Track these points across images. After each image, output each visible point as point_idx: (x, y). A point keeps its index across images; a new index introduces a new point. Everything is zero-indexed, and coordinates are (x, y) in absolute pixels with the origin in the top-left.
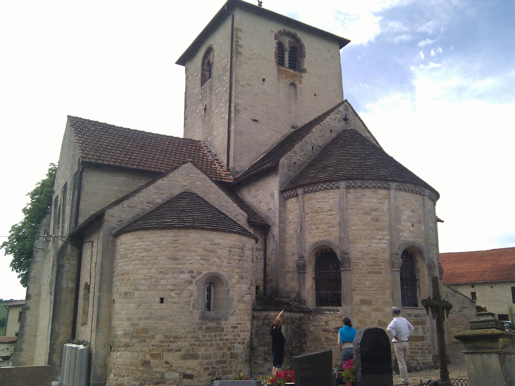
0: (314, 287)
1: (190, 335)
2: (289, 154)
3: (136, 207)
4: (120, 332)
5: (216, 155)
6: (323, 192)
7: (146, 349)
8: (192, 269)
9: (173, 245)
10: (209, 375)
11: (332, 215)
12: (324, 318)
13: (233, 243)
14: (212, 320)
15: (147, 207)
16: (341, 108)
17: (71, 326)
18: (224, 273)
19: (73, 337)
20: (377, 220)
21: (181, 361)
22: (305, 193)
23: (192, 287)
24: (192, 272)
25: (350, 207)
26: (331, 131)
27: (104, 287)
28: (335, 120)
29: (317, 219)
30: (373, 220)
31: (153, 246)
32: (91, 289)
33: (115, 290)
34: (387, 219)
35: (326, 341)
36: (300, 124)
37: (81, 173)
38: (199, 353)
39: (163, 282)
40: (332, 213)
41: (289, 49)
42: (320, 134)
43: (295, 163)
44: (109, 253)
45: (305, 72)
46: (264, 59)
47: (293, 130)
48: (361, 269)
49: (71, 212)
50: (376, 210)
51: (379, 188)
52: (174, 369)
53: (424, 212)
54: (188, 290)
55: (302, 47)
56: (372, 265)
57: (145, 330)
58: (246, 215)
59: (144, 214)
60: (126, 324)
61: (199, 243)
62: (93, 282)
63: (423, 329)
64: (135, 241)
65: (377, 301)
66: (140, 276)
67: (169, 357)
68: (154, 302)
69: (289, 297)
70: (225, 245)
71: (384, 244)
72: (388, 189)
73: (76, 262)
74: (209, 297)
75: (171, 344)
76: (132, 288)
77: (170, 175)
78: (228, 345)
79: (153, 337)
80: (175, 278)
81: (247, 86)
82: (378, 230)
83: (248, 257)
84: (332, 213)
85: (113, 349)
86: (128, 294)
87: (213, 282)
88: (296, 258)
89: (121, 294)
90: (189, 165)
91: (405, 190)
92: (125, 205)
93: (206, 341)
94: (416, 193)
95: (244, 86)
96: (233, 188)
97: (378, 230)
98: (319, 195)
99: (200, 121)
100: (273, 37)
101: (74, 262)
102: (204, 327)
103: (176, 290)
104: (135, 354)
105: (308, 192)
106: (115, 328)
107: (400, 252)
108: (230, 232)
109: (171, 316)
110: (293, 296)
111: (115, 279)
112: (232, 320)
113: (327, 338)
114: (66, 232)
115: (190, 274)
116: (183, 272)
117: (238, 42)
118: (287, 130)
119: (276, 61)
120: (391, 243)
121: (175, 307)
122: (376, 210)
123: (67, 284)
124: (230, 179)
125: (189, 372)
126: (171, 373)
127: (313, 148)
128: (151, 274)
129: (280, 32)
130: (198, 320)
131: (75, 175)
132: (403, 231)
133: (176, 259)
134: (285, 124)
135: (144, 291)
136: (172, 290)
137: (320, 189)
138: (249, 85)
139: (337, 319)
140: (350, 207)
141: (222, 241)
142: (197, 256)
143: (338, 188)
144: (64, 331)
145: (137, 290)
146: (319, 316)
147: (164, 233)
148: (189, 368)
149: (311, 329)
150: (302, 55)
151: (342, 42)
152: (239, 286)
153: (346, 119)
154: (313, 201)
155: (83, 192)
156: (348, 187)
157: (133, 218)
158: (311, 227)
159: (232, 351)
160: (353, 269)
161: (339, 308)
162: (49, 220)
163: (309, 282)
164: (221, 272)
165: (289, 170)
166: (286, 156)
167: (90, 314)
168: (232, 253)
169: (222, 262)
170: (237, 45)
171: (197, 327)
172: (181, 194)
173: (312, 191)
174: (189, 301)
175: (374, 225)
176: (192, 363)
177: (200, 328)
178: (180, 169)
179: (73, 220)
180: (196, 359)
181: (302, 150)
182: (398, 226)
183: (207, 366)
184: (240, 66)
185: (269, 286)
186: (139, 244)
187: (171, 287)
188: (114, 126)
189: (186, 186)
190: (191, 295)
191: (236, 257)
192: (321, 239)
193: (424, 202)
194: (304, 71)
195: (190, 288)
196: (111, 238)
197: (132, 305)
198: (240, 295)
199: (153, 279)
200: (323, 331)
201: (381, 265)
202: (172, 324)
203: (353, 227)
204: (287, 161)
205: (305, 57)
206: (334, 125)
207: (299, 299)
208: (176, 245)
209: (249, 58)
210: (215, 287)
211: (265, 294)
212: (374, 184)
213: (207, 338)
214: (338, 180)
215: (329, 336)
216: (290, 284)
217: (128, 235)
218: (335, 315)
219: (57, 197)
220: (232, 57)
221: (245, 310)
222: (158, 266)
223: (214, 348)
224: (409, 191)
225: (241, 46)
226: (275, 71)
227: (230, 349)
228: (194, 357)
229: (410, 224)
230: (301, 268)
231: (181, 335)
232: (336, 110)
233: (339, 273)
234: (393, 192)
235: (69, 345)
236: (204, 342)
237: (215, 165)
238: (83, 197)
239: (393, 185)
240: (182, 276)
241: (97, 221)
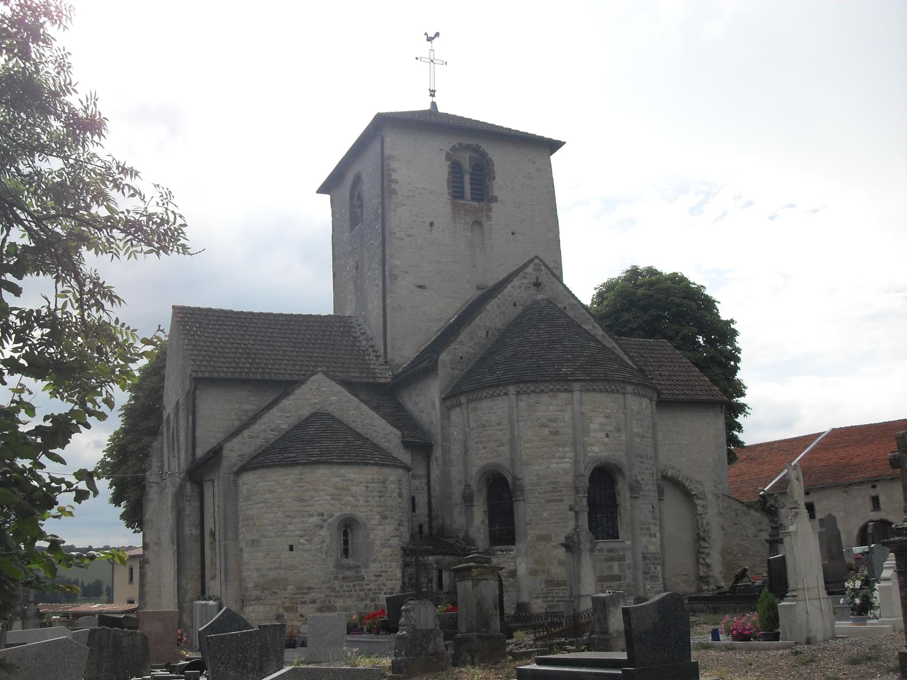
0: (487, 522)
1: (325, 586)
2: (453, 346)
3: (258, 437)
4: (250, 585)
5: (371, 339)
11: (501, 430)
13: (370, 476)
14: (350, 568)
16: (530, 269)
17: (200, 580)
18: (361, 514)
19: (203, 594)
20: (557, 433)
22: (469, 401)
23: (323, 532)
24: (322, 514)
26: (515, 305)
30: (551, 433)
32: (217, 537)
33: (241, 537)
34: (570, 431)
36: (491, 282)
37: (194, 393)
38: (337, 605)
39: (290, 527)
40: (501, 427)
41: (470, 170)
43: (461, 358)
44: (232, 494)
45: (496, 201)
47: (480, 293)
48: (537, 498)
49: (187, 442)
50: (555, 420)
51: (558, 390)
53: (625, 415)
56: (550, 492)
58: (399, 433)
59: (268, 445)
61: (328, 480)
62: (217, 528)
63: (620, 566)
65: (558, 535)
67: (302, 609)
69: (457, 536)
71: (567, 464)
72: (571, 391)
73: (198, 504)
74: (346, 542)
75: (305, 596)
78: (371, 595)
79: (285, 589)
80: (303, 522)
83: (393, 492)
84: (501, 427)
87: (348, 527)
90: (320, 376)
91: (594, 390)
94: (613, 391)
95: (402, 239)
96: (387, 395)
97: (558, 446)
98: (485, 404)
100: (444, 158)
101: (196, 504)
102: (340, 576)
105: (472, 400)
107: (588, 474)
108: (366, 464)
110: (462, 535)
111: (240, 525)
112: (375, 567)
114: (184, 466)
116: (312, 515)
117: (390, 175)
118: (470, 294)
120: (576, 462)
122: (555, 420)
123: (190, 530)
124: (386, 377)
127: (487, 332)
129: (454, 149)
131: (187, 394)
132: (592, 445)
134: (468, 285)
136: (301, 536)
137: (486, 397)
141: (356, 476)
142: (327, 495)
143: (506, 394)
144: (192, 586)
145: (264, 537)
147: (289, 470)
152: (382, 527)
153: (537, 284)
155: (198, 416)
156: (518, 393)
157: (255, 451)
159: (377, 602)
162: (162, 442)
163: (479, 515)
164: (357, 513)
165: (453, 369)
166: (448, 349)
167: (218, 566)
168: (370, 489)
169: (358, 501)
170: (391, 181)
172: (314, 414)
173: (476, 399)
177: (336, 578)
178: (309, 382)
179: (190, 453)
182: (586, 439)
185: (434, 524)
188: (232, 312)
190: (323, 542)
191: (375, 493)
192: (489, 461)
193: (625, 403)
194: (495, 199)
196: (232, 476)
198: (384, 539)
202: (305, 573)
203: (526, 445)
205: (494, 178)
209: (408, 197)
210: (352, 531)
211: (431, 534)
212: (551, 387)
213: (345, 588)
216: (457, 520)
217: (250, 473)
219: (169, 416)
220: (383, 199)
221: (391, 555)
224: (601, 391)
225: (396, 181)
226: (448, 208)
227: (373, 600)
228: (332, 609)
229: (603, 435)
230: (468, 499)
232: (522, 274)
233: (512, 503)
234: (577, 395)
235: (199, 602)
236: (342, 593)
237: (369, 355)
238: (199, 421)
239: (577, 386)
240: (311, 520)
241: (216, 454)
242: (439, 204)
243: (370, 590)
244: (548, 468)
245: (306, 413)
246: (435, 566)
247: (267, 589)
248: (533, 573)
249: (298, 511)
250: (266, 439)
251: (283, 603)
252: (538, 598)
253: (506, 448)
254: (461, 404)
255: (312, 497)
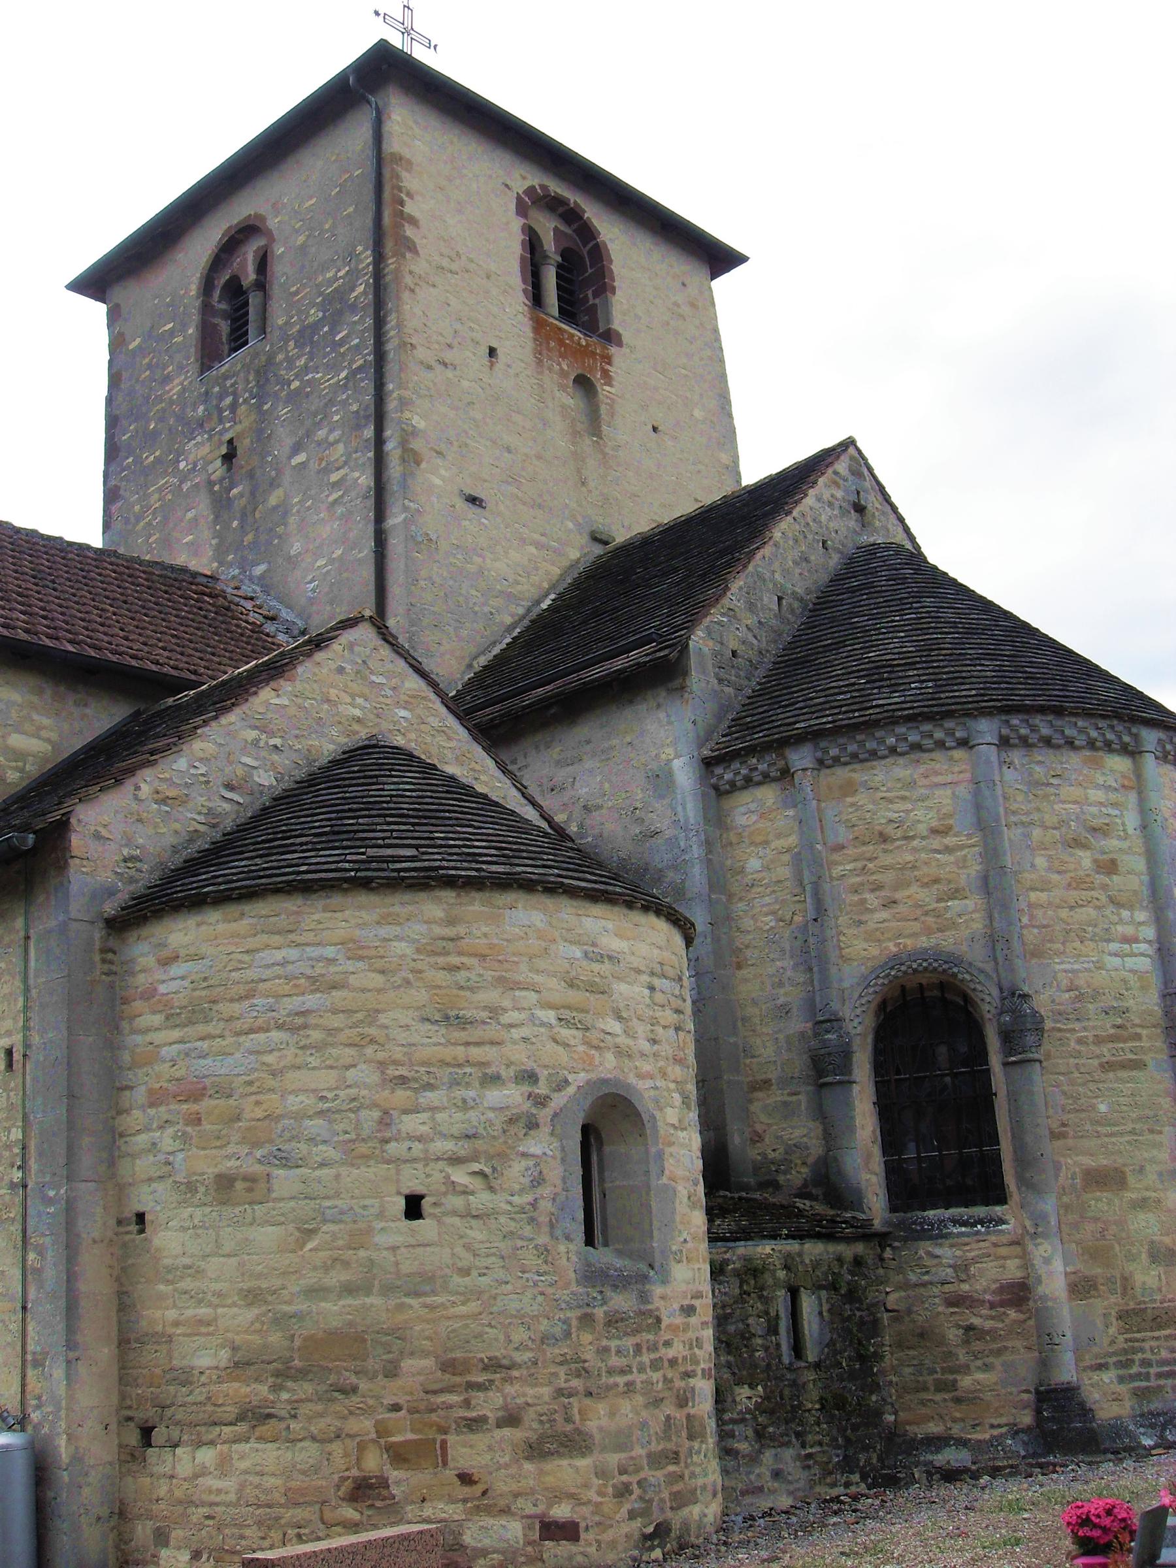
2: (716, 615)
6: (901, 761)
7: (366, 1425)
8: (530, 1065)
9: (441, 960)
10: (632, 1515)
11: (948, 850)
12: (946, 1253)
14: (621, 1282)
15: (227, 806)
16: (842, 466)
21: (528, 1466)
23: (539, 1145)
24: (531, 1077)
25: (1013, 819)
27: (87, 1161)
28: (830, 504)
29: (886, 868)
31: (350, 966)
34: (1140, 865)
35: (967, 1342)
38: (592, 1426)
39: (411, 1124)
40: (950, 841)
42: (796, 554)
43: (734, 654)
45: (620, 344)
46: (488, 277)
47: (598, 550)
48: (1078, 1055)
51: (1108, 746)
52: (502, 1503)
54: (524, 1155)
55: (598, 254)
56: (1112, 1039)
57: (350, 1342)
60: (239, 1319)
64: (252, 943)
66: (294, 1102)
67: (468, 1452)
68: (381, 1215)
70: (636, 962)
71: (1142, 961)
72: (1132, 752)
75: (478, 1397)
76: (259, 1153)
77: (300, 669)
79: (392, 1371)
80: (465, 1106)
81: (439, 368)
82: (1119, 905)
84: (950, 841)
85: (159, 1436)
86: (239, 1185)
88: (798, 1024)
89: (191, 1187)
92: (146, 789)
93: (610, 1372)
98: (889, 775)
99: (202, 507)
102: (599, 1312)
103: (474, 1158)
104: (308, 1453)
106: (170, 1339)
109: (466, 1272)
110: (798, 1175)
113: (970, 1328)
115: (526, 1088)
116: (494, 1080)
119: (525, 291)
121: (476, 1233)
125: (562, 1512)
126: (489, 1521)
127: (780, 599)
128: (353, 1092)
130: (574, 1287)
133: (463, 1023)
135: (322, 1165)
136: (456, 1160)
137: (893, 751)
138: (445, 365)
139: (1003, 1251)
140: (1013, 819)
143: (964, 743)
145: (285, 1161)
146: (924, 1247)
147: (399, 904)
148: (558, 1496)
149: (893, 1300)
150: (602, 283)
151: (719, 258)
154: (861, 798)
156: (1004, 743)
158: (863, 902)
160: (1048, 1056)
161: (998, 1209)
164: (632, 1079)
165: (720, 681)
171: (573, 1315)
174: (534, 1205)
175: (1104, 887)
176: (567, 1471)
177: (587, 1320)
180: (583, 1455)
181: (751, 607)
183: (624, 1478)
184: (412, 291)
186: (279, 955)
187: (449, 1146)
189: (359, 720)
190: (538, 1181)
195: (532, 1150)
196: (98, 934)
197: (267, 1235)
199: (364, 1113)
200: (950, 1303)
201: (1138, 1037)
202: (473, 1306)
203: (1033, 896)
204: (711, 643)
206: (831, 525)
207: (828, 1183)
208: (455, 960)
213: (615, 1361)
214: (968, 714)
215: (976, 1321)
218: (993, 1238)
222: (381, 1055)
223: (640, 1399)
225: (413, 221)
228: (573, 1443)
231: (519, 1357)
240: (494, 1096)
242: (506, 311)
243: (673, 1362)
244: (1100, 966)
245: (327, 745)
246: (781, 1274)
247: (302, 1374)
248: (1081, 1288)
249: (444, 1063)
250: (210, 812)
251: (382, 1430)
252: (1101, 1367)
253: (970, 904)
254: (786, 774)
255: (495, 1011)
